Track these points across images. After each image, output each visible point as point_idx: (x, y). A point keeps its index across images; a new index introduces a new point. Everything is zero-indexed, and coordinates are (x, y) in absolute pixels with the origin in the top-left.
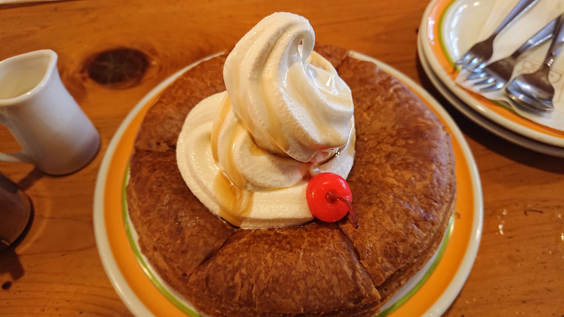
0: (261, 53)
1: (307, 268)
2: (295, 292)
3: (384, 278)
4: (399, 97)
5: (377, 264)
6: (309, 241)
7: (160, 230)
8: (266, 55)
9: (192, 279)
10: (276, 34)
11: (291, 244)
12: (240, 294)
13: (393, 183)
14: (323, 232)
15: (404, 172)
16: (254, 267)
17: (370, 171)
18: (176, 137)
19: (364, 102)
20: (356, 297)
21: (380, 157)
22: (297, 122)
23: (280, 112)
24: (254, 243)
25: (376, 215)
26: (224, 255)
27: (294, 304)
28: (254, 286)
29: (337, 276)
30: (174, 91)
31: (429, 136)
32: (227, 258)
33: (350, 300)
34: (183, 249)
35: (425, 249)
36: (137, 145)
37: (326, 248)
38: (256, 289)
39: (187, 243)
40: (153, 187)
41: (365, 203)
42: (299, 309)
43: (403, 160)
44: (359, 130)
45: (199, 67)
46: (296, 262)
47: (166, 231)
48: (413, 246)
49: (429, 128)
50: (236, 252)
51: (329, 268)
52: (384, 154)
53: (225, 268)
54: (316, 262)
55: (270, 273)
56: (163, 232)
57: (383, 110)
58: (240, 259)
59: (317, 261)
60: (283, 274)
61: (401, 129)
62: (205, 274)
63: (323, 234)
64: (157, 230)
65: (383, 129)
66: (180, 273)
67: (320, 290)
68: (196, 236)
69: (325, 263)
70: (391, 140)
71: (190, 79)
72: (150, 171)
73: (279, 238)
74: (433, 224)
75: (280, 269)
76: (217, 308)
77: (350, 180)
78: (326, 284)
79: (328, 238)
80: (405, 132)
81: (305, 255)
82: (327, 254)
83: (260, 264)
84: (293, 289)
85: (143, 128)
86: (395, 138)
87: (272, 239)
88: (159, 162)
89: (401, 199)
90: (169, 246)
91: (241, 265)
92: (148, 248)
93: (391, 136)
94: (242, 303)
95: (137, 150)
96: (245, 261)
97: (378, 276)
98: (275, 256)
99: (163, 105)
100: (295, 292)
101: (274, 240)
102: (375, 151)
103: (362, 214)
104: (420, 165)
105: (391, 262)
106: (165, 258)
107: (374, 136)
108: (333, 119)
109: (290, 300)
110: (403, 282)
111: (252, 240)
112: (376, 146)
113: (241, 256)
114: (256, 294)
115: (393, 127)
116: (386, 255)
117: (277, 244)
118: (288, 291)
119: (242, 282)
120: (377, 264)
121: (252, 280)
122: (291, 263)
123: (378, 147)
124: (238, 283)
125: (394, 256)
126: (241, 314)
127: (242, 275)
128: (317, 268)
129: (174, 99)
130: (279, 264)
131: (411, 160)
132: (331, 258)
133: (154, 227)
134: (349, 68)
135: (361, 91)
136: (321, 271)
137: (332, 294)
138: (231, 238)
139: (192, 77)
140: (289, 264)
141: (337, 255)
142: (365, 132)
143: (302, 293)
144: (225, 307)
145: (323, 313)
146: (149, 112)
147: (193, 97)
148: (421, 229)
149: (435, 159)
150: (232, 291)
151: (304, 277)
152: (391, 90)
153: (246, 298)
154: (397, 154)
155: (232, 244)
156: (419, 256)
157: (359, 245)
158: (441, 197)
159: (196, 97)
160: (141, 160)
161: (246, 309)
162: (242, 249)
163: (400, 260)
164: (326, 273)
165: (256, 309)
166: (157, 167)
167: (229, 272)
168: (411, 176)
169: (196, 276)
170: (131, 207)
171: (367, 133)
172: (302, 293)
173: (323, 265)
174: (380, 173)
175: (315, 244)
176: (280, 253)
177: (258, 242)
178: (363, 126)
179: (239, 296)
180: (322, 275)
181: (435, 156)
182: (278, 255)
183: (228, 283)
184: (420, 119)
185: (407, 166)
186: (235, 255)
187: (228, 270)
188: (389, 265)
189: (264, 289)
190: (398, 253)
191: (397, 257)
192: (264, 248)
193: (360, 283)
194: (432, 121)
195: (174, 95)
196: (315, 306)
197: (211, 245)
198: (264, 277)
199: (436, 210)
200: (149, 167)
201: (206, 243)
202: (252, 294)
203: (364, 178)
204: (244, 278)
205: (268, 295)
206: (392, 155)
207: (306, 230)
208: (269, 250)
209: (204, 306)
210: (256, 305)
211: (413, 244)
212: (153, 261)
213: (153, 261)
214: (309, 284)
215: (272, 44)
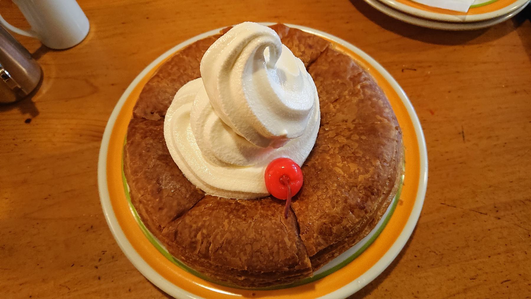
0: (229, 58)
1: (255, 235)
2: (242, 253)
3: (316, 251)
4: (364, 94)
5: (312, 239)
6: (261, 213)
7: (144, 188)
8: (234, 59)
9: (165, 231)
10: (242, 44)
11: (246, 214)
12: (199, 249)
13: (340, 173)
14: (274, 206)
15: (351, 165)
17: (324, 159)
18: (167, 107)
20: (291, 263)
21: (335, 148)
22: (256, 118)
23: (242, 107)
24: (217, 209)
25: (320, 198)
26: (191, 216)
27: (240, 262)
29: (278, 244)
30: (170, 67)
31: (381, 134)
32: (193, 218)
33: (285, 265)
34: (160, 206)
35: (356, 231)
36: (135, 112)
37: (273, 221)
38: (212, 247)
39: (163, 202)
40: (143, 152)
41: (313, 187)
42: (243, 267)
43: (353, 153)
44: (324, 120)
45: (194, 46)
46: (247, 229)
47: (149, 190)
48: (345, 228)
49: (384, 127)
50: (201, 215)
51: (272, 237)
52: (338, 146)
53: (191, 227)
54: (263, 231)
55: (225, 236)
56: (146, 191)
57: (348, 104)
58: (204, 221)
59: (264, 231)
60: (235, 238)
61: (360, 124)
62: (174, 229)
63: (273, 209)
64: (142, 189)
66: (157, 224)
67: (262, 254)
68: (172, 197)
70: (347, 133)
71: (185, 57)
72: (142, 138)
73: (238, 207)
74: (366, 212)
75: (233, 234)
76: (182, 256)
77: (307, 165)
78: (268, 251)
79: (277, 213)
80: (362, 128)
81: (255, 225)
82: (273, 226)
83: (218, 228)
84: (241, 250)
85: (141, 98)
86: (352, 132)
87: (232, 207)
88: (150, 131)
89: (344, 188)
90: (150, 202)
91: (203, 226)
92: (136, 200)
93: (349, 129)
94: (201, 256)
95: (135, 115)
96: (207, 223)
97: (312, 248)
98: (231, 222)
99: (160, 79)
100: (242, 253)
101: (233, 208)
102: (332, 141)
103: (309, 196)
104: (366, 160)
105: (324, 239)
106: (147, 211)
107: (336, 127)
108: (290, 116)
109: (238, 258)
110: (336, 254)
111: (216, 206)
112: (334, 137)
113: (204, 219)
114: (212, 251)
115: (354, 121)
116: (321, 233)
118: (237, 252)
119: (202, 240)
120: (312, 239)
121: (211, 239)
122: (243, 230)
123: (336, 138)
124: (199, 240)
125: (327, 235)
126: (200, 263)
127: (203, 234)
128: (263, 236)
129: (169, 74)
130: (233, 229)
131: (360, 154)
132: (276, 230)
133: (140, 185)
134: (326, 60)
135: (332, 83)
136: (266, 239)
137: (271, 259)
138: (200, 201)
139: (187, 56)
140: (241, 231)
141: (281, 228)
142: (329, 121)
143: (248, 255)
144: (188, 256)
145: (262, 272)
146: (147, 84)
147: (185, 74)
148: (355, 215)
149: (381, 156)
150: (194, 245)
151: (252, 243)
152: (359, 87)
153: (204, 253)
154: (350, 147)
155: (199, 207)
156: (350, 236)
157: (302, 222)
158: (378, 190)
159: (188, 75)
160: (137, 126)
161: (204, 260)
162: (206, 213)
163: (332, 238)
165: (211, 262)
166: (148, 134)
167: (194, 230)
168: (357, 169)
169: (168, 230)
170: (126, 165)
173: (268, 235)
174: (330, 163)
175: (265, 216)
176: (236, 221)
177: (220, 209)
178: (329, 117)
179: (199, 250)
180: (266, 243)
181: (382, 154)
182: (233, 222)
183: (192, 239)
184: (379, 117)
185: (354, 158)
186: (200, 217)
187: (193, 228)
188: (322, 241)
189: (218, 247)
190: (331, 232)
191: (330, 236)
192: (224, 214)
193: (296, 252)
194: (388, 120)
195: (170, 71)
196: (256, 266)
197: (183, 206)
198: (220, 238)
199: (372, 201)
200: (142, 133)
201: (179, 204)
202: (208, 251)
203: (317, 164)
204: (204, 237)
205: (221, 252)
206: (345, 147)
207: (261, 204)
208: (227, 217)
209: (173, 252)
210: (211, 259)
211: (345, 226)
212: (139, 211)
213: (139, 211)
215: (239, 52)
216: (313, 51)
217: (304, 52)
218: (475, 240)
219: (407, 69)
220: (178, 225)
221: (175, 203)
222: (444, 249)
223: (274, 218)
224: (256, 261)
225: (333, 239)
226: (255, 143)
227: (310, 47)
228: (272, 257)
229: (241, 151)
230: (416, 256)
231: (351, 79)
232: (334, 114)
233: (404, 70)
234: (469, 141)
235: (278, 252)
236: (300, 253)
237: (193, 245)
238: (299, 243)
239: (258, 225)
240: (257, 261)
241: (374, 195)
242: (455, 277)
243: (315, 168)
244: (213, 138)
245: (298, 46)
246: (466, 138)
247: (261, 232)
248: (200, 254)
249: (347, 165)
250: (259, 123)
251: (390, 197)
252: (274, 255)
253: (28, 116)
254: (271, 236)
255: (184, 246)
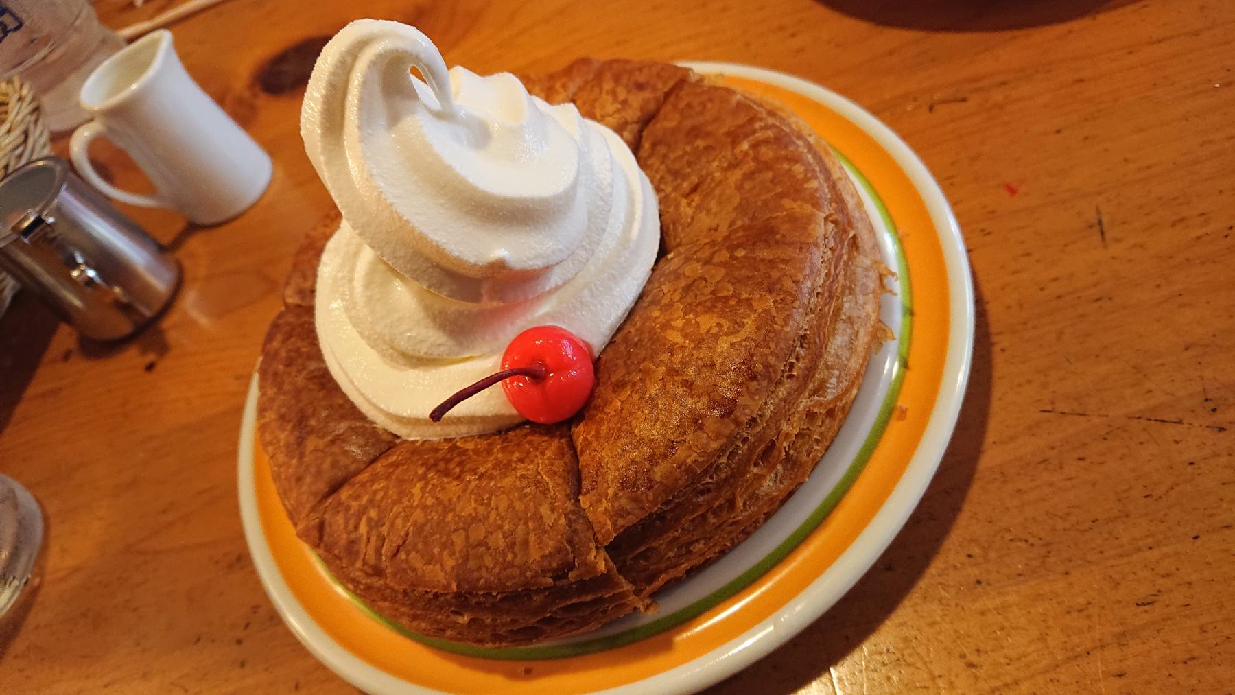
3: (615, 530)
10: (339, 65)
14: (530, 442)
16: (391, 506)
19: (685, 177)
20: (555, 565)
28: (386, 541)
29: (526, 524)
43: (713, 293)
46: (459, 497)
47: (282, 443)
48: (683, 468)
62: (317, 518)
63: (527, 446)
64: (270, 443)
65: (712, 231)
68: (322, 451)
69: (509, 499)
75: (429, 511)
84: (444, 547)
97: (606, 524)
108: (500, 214)
109: (438, 566)
117: (442, 465)
118: (436, 550)
122: (450, 500)
127: (370, 520)
128: (493, 509)
134: (675, 106)
135: (686, 153)
136: (498, 514)
137: (510, 559)
140: (446, 502)
151: (467, 526)
156: (709, 491)
164: (506, 518)
171: (684, 241)
172: (458, 555)
185: (716, 303)
196: (478, 580)
202: (380, 555)
214: (471, 540)
216: (647, 94)
217: (625, 102)
218: (1146, 497)
219: (944, 102)
220: (326, 507)
221: (327, 465)
222: (1054, 530)
223: (523, 465)
224: (476, 568)
225: (657, 498)
226: (445, 293)
227: (640, 87)
228: (512, 556)
229: (436, 321)
230: (970, 556)
231: (728, 134)
232: (689, 220)
233: (935, 108)
234: (1118, 240)
235: (526, 543)
236: (576, 539)
237: (351, 548)
238: (574, 515)
239: (484, 484)
240: (479, 568)
241: (758, 381)
242: (1089, 603)
243: (627, 343)
244: (370, 299)
245: (613, 93)
246: (1109, 235)
247: (490, 499)
248: (366, 567)
249: (693, 322)
250: (422, 237)
251: (829, 390)
252: (515, 550)
253: (151, 357)
254: (511, 506)
255: (336, 552)
